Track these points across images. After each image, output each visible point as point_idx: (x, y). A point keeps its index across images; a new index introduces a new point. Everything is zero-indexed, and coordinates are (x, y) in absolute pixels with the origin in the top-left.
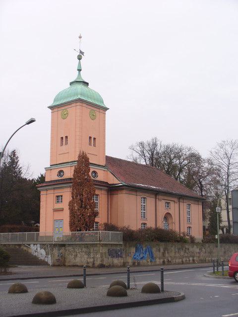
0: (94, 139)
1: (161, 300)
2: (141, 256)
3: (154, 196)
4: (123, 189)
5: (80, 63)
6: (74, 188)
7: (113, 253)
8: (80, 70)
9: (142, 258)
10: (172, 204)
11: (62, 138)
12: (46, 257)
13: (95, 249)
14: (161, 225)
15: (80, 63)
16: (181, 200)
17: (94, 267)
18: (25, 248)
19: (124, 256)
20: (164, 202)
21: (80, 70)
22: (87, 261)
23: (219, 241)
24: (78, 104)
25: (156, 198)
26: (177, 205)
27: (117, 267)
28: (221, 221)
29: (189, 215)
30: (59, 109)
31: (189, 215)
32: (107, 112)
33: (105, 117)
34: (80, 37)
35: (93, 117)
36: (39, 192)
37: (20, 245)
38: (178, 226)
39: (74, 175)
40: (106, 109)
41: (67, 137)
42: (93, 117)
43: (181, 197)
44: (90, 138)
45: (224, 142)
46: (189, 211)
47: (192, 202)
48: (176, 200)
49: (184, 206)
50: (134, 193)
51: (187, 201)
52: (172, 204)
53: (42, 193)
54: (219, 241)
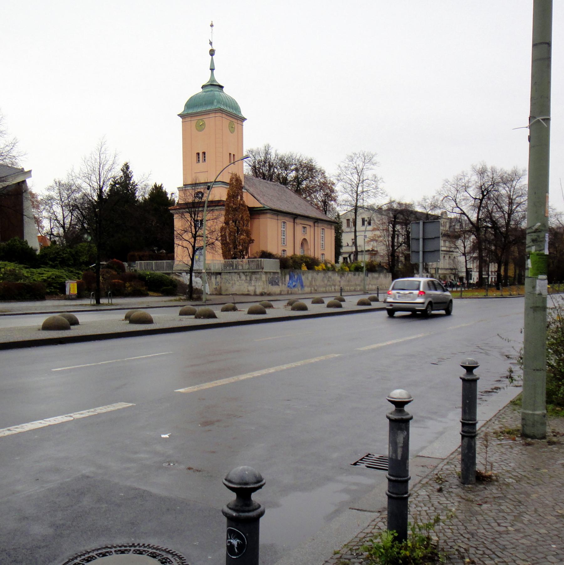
0: (234, 155)
1: (182, 327)
2: (294, 284)
3: (292, 220)
4: (267, 213)
5: (212, 59)
6: (227, 213)
7: (273, 282)
8: (212, 69)
9: (294, 286)
10: (326, 230)
11: (198, 154)
12: (202, 285)
13: (258, 276)
14: (299, 253)
15: (212, 59)
16: (316, 224)
17: (255, 295)
18: (175, 277)
19: (280, 284)
20: (301, 226)
21: (212, 69)
22: (248, 289)
23: (365, 269)
24: (219, 114)
25: (294, 222)
26: (312, 229)
27: (275, 294)
28: (528, 264)
29: (284, 236)
30: (193, 119)
31: (284, 236)
32: (245, 123)
33: (242, 128)
34: (212, 26)
35: (232, 129)
36: (172, 216)
37: (169, 274)
38: (313, 252)
39: (227, 199)
40: (244, 119)
41: (204, 153)
42: (232, 129)
43: (316, 221)
44: (230, 154)
45: (355, 154)
46: (323, 237)
47: (326, 226)
48: (311, 223)
49: (319, 229)
50: (275, 217)
51: (322, 225)
52: (326, 230)
53: (176, 216)
54: (365, 269)
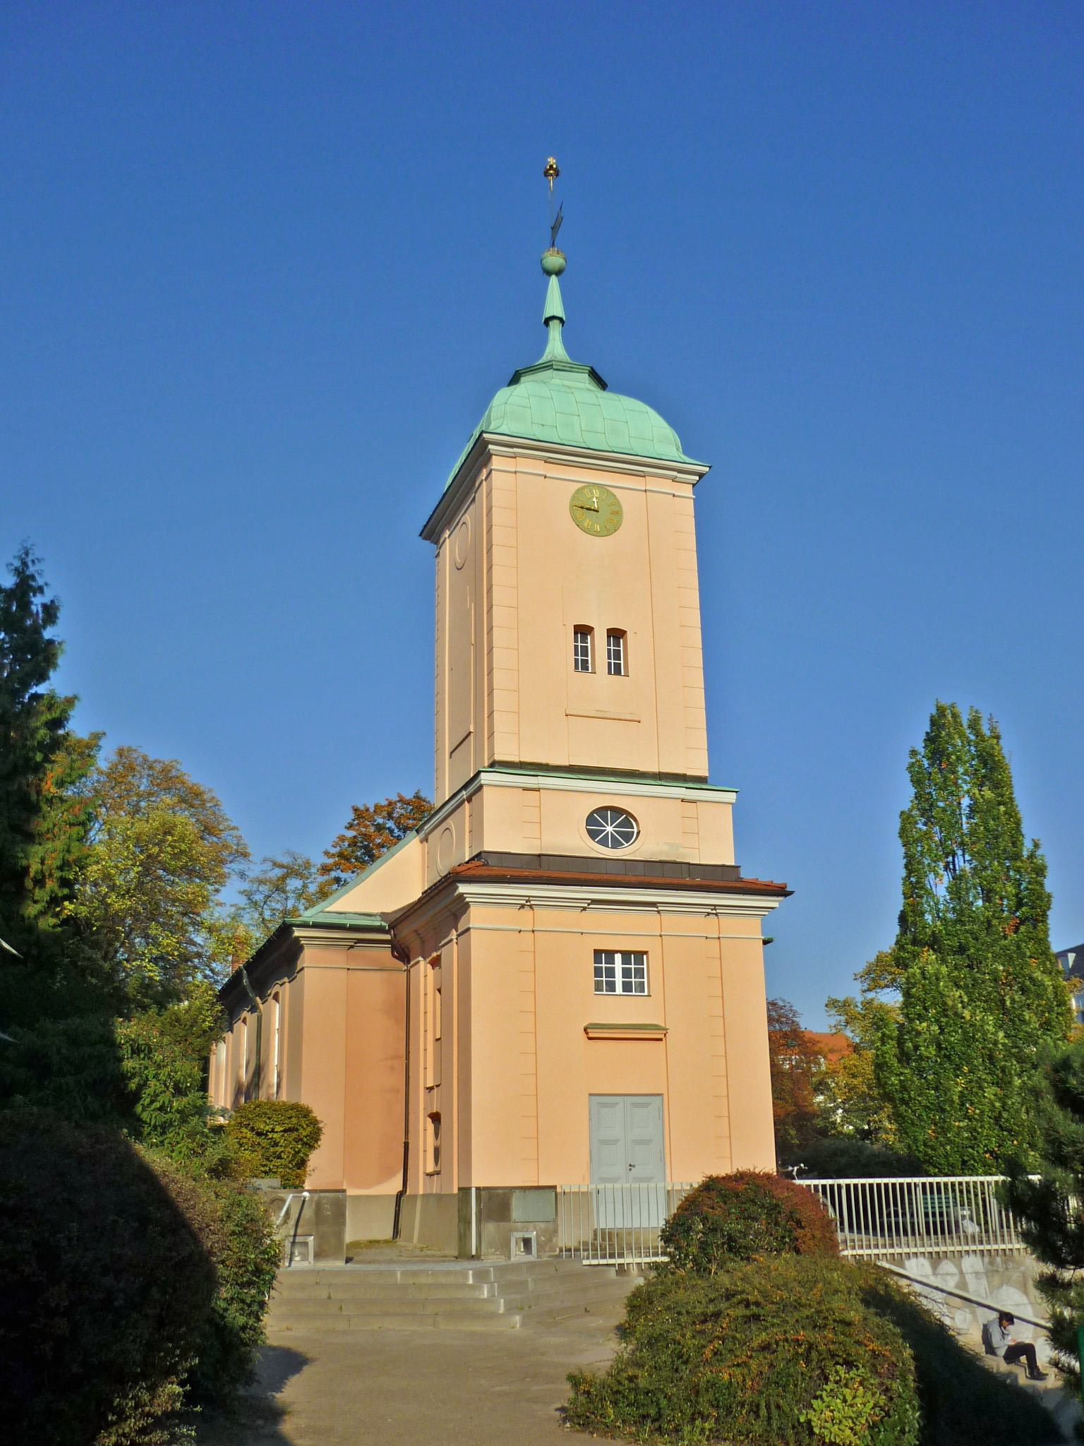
0: (616, 635)
44: (583, 631)
